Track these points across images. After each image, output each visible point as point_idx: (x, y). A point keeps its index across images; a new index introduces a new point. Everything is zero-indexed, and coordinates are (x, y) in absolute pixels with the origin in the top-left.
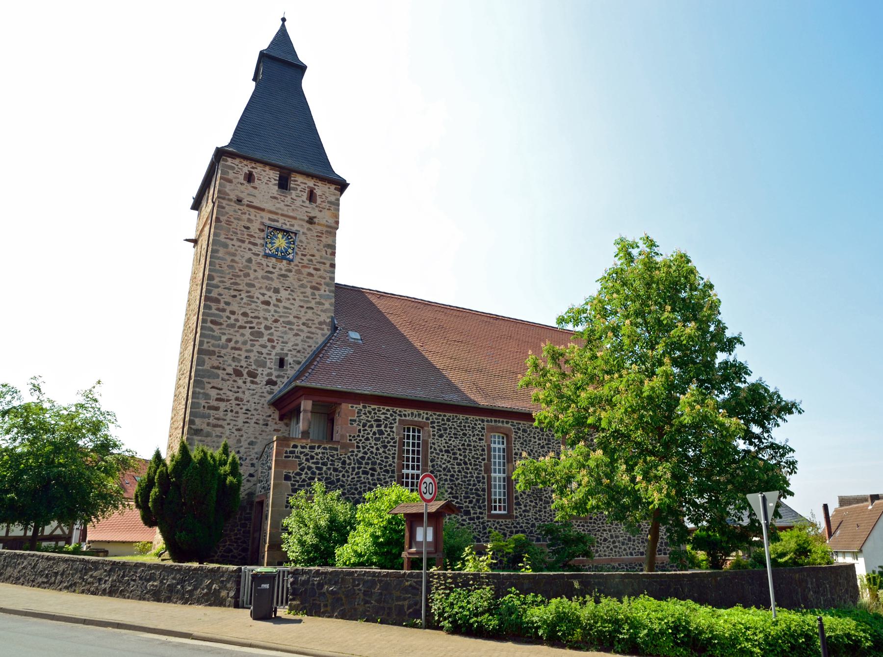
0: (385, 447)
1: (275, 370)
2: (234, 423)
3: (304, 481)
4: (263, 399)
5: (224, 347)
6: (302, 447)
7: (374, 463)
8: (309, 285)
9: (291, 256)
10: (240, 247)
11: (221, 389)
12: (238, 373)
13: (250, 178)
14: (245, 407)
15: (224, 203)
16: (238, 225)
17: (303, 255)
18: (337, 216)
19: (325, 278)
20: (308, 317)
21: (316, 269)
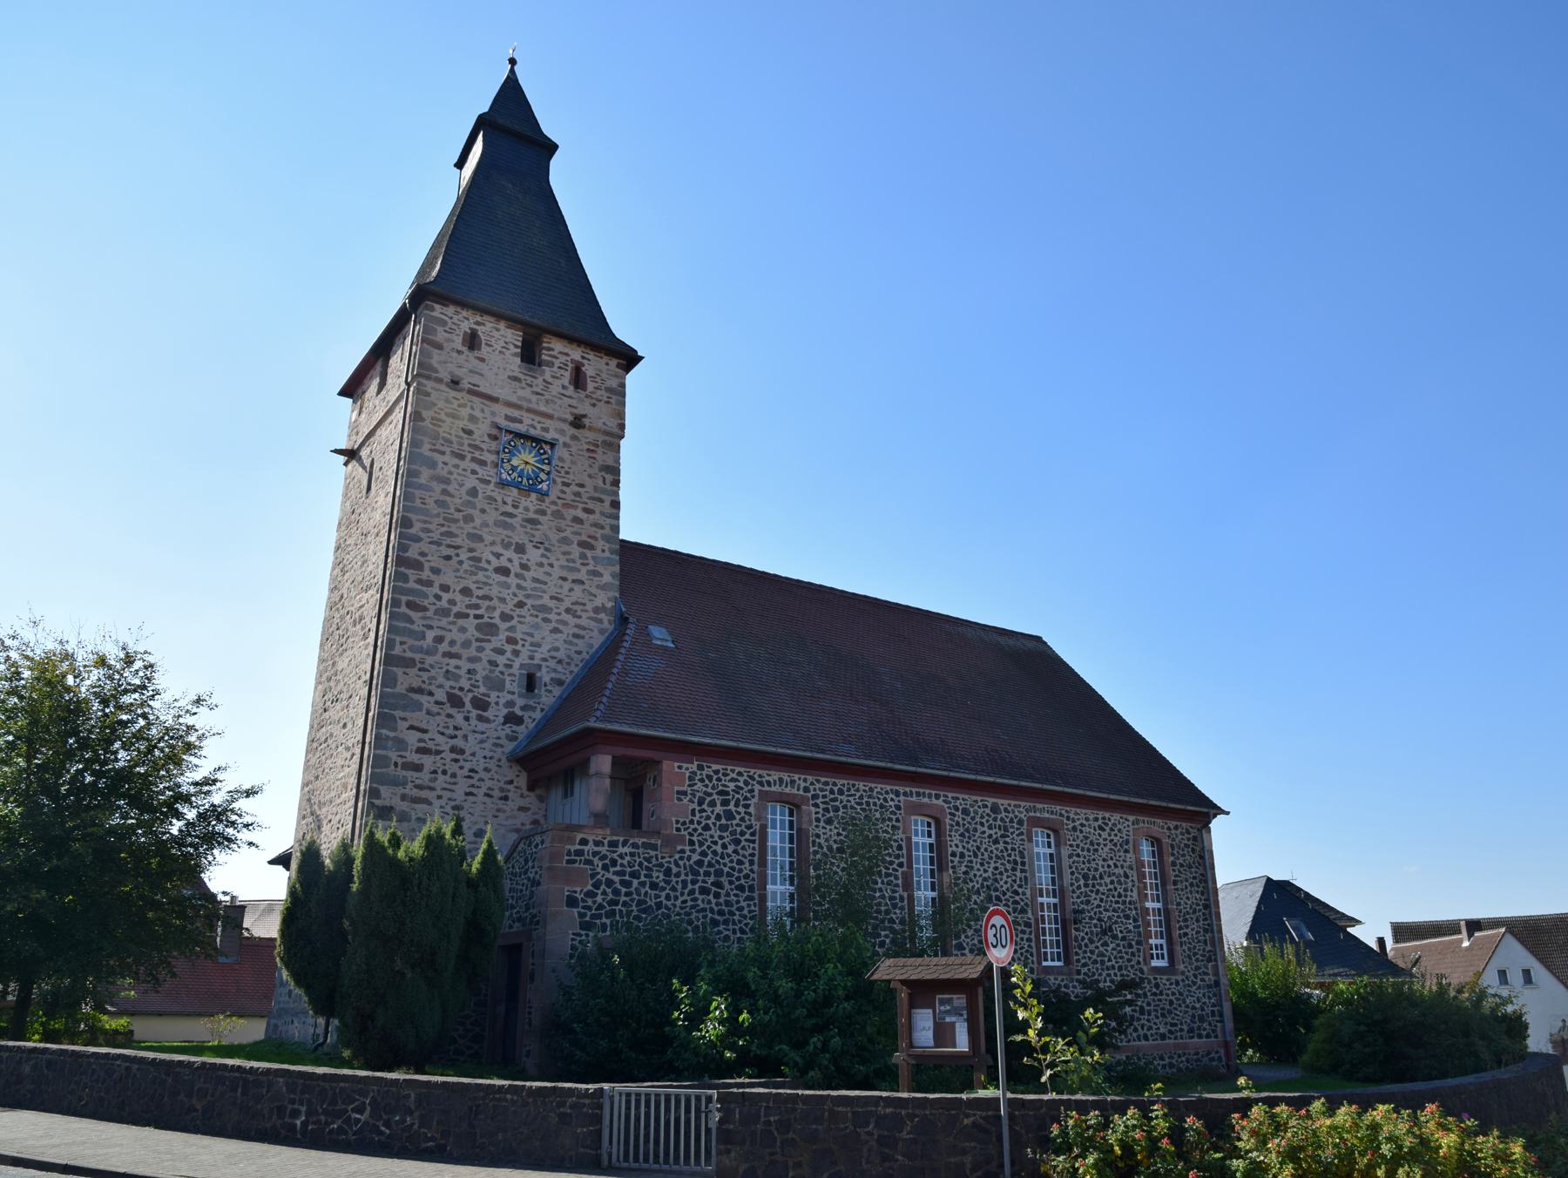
0: (737, 842)
1: (520, 695)
2: (449, 794)
3: (600, 907)
4: (499, 750)
5: (429, 652)
6: (597, 843)
7: (719, 873)
8: (575, 539)
9: (544, 486)
10: (457, 466)
11: (425, 731)
12: (456, 701)
13: (472, 341)
14: (468, 766)
15: (429, 385)
16: (451, 429)
17: (564, 484)
18: (621, 415)
19: (602, 528)
20: (574, 599)
21: (588, 511)
